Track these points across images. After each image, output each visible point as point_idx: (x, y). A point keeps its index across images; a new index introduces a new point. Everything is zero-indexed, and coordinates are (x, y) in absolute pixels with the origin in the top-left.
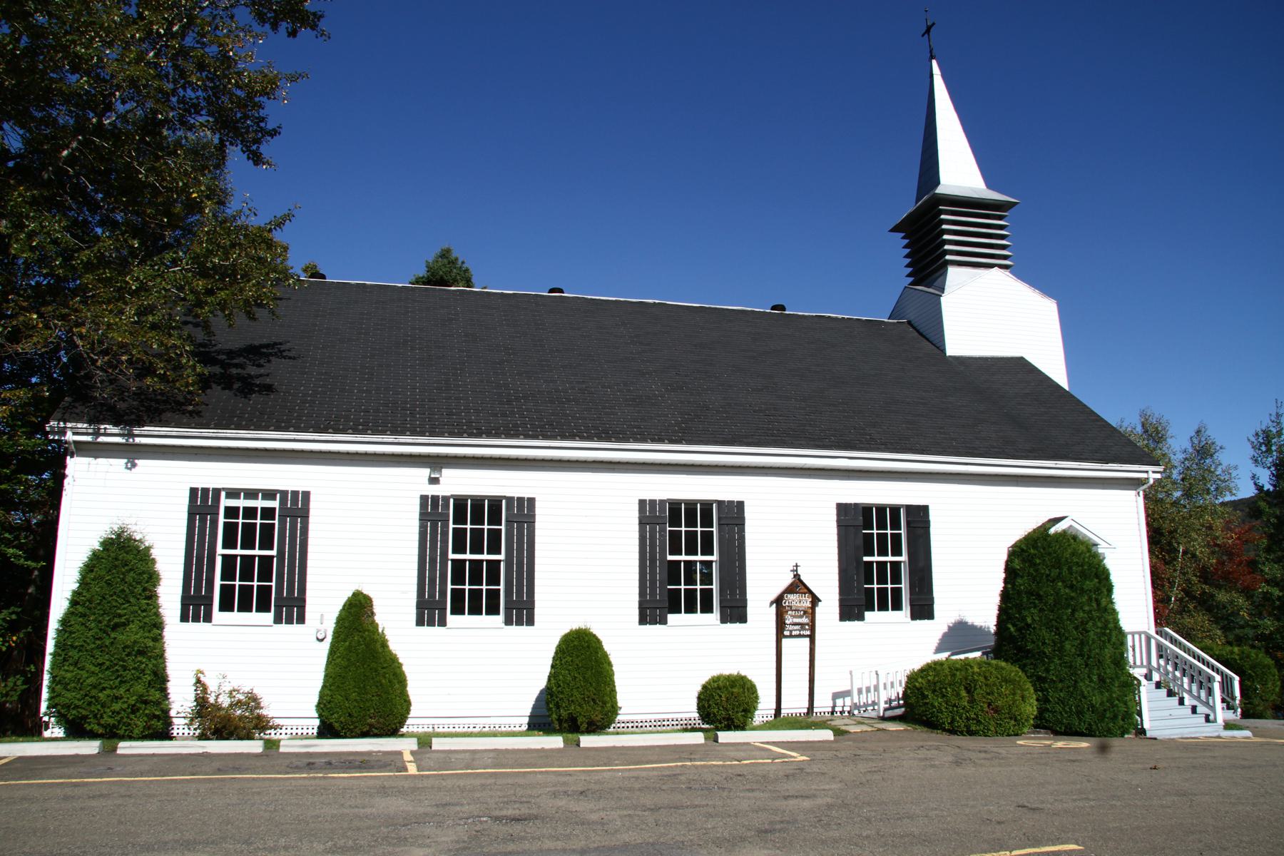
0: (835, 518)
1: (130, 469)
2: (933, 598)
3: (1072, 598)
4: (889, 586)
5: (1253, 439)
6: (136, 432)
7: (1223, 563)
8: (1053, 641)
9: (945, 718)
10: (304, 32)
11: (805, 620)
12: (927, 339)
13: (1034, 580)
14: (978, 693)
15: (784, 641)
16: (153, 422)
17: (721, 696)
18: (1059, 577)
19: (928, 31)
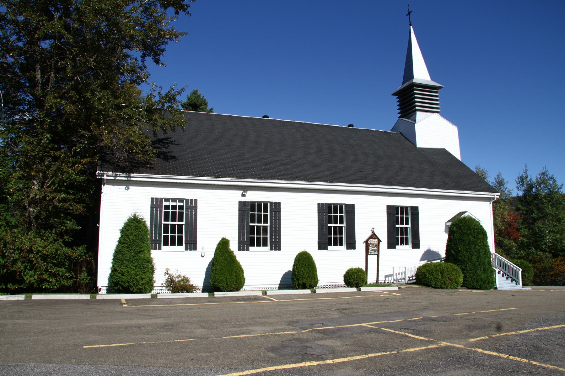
0: (386, 211)
1: (127, 190)
2: (355, 241)
3: (475, 241)
4: (338, 236)
5: (517, 180)
6: (132, 176)
7: (507, 228)
8: (468, 256)
9: (433, 283)
10: (181, 12)
11: (376, 248)
12: (408, 140)
13: (461, 235)
14: (445, 274)
15: (369, 256)
16: (136, 172)
17: (354, 276)
18: (470, 234)
19: (409, 14)
